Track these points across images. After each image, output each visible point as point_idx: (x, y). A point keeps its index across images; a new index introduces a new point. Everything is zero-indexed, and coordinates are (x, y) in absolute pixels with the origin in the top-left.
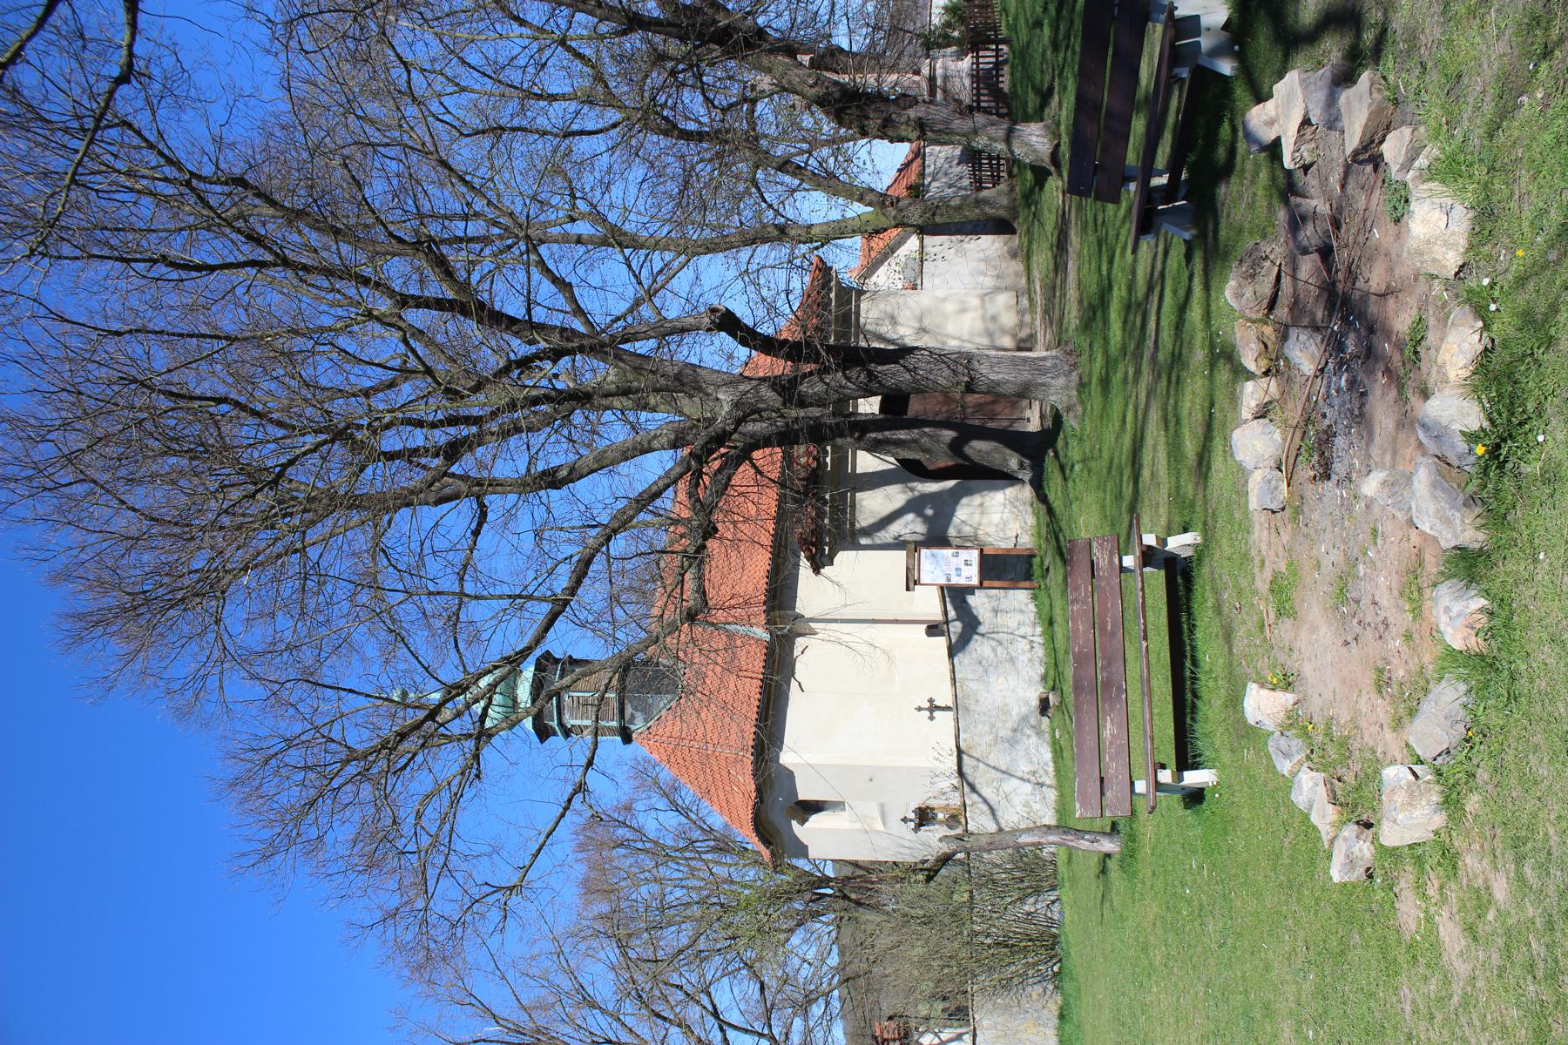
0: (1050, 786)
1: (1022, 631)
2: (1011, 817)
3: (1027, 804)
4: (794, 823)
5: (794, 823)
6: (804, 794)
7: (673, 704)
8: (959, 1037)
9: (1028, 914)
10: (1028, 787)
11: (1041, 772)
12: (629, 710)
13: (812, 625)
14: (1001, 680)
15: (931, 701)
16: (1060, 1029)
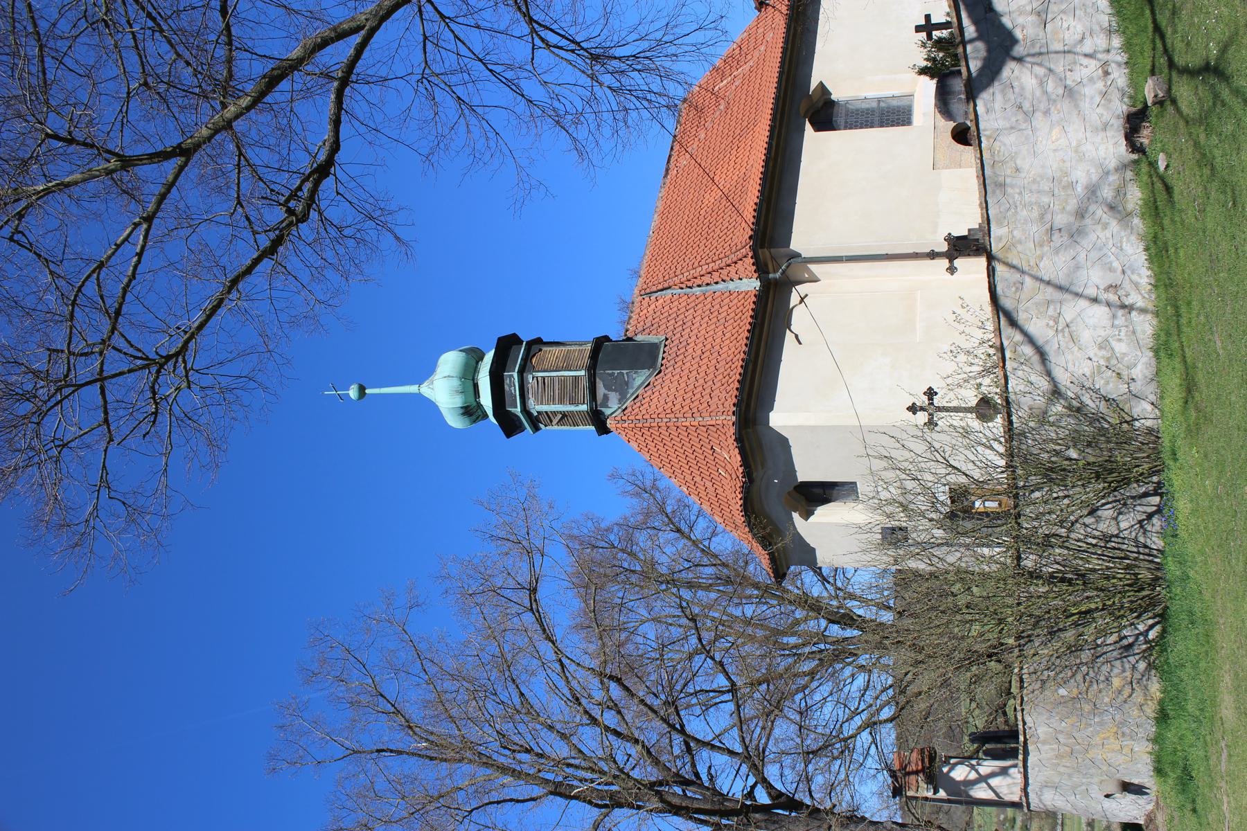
0: (1143, 311)
1: (1087, 47)
2: (1073, 366)
3: (1104, 344)
4: (796, 516)
5: (796, 516)
6: (805, 473)
7: (652, 379)
8: (1004, 772)
9: (1107, 538)
10: (1101, 312)
11: (1127, 285)
12: (601, 390)
13: (813, 267)
14: (1056, 132)
15: (918, 29)
16: (1157, 740)
